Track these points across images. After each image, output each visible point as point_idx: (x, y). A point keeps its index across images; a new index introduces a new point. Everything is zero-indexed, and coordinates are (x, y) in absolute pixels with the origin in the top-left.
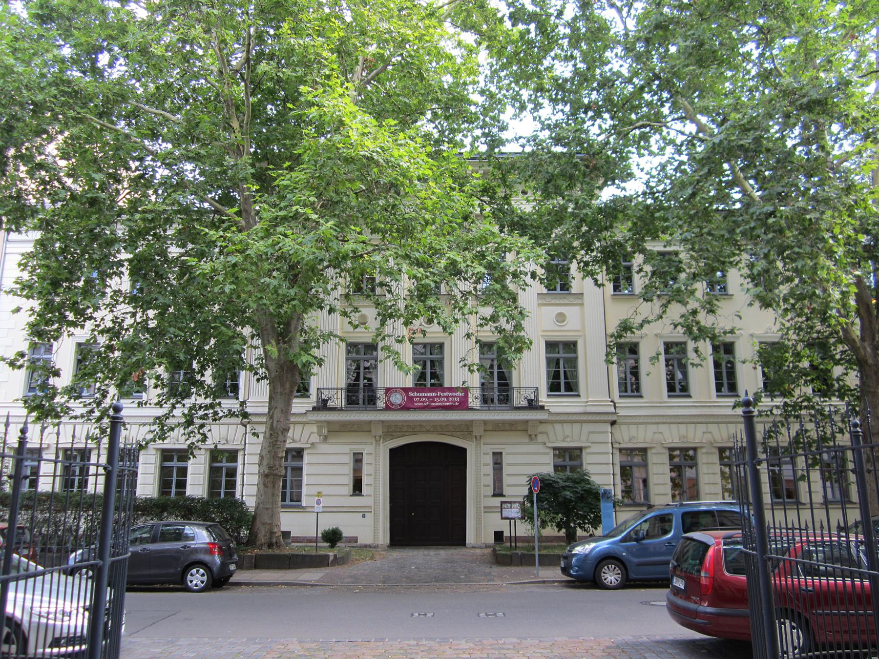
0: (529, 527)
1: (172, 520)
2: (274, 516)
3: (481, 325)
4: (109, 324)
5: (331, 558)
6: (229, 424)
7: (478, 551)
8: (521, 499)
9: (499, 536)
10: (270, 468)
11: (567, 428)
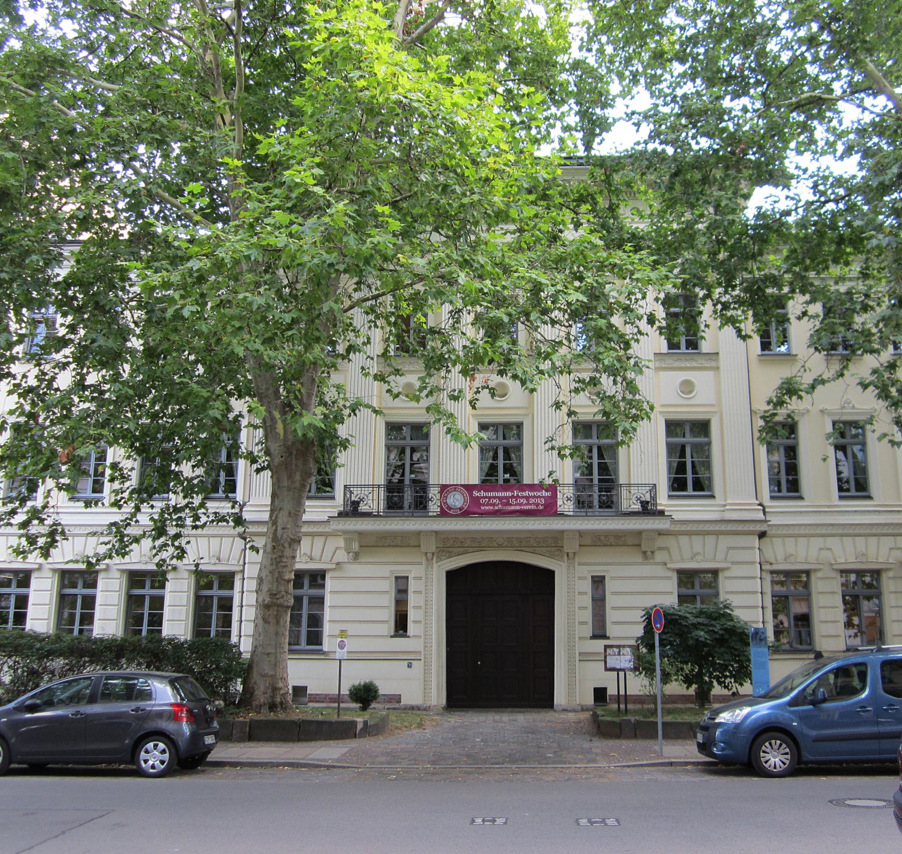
0: (646, 682)
1: (131, 670)
2: (278, 664)
3: (576, 391)
4: (32, 382)
5: (360, 726)
6: (221, 536)
7: (571, 716)
8: (633, 642)
9: (600, 694)
10: (272, 595)
11: (697, 541)
